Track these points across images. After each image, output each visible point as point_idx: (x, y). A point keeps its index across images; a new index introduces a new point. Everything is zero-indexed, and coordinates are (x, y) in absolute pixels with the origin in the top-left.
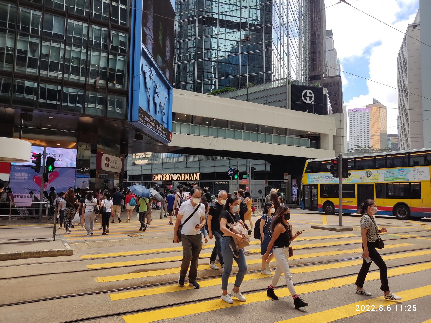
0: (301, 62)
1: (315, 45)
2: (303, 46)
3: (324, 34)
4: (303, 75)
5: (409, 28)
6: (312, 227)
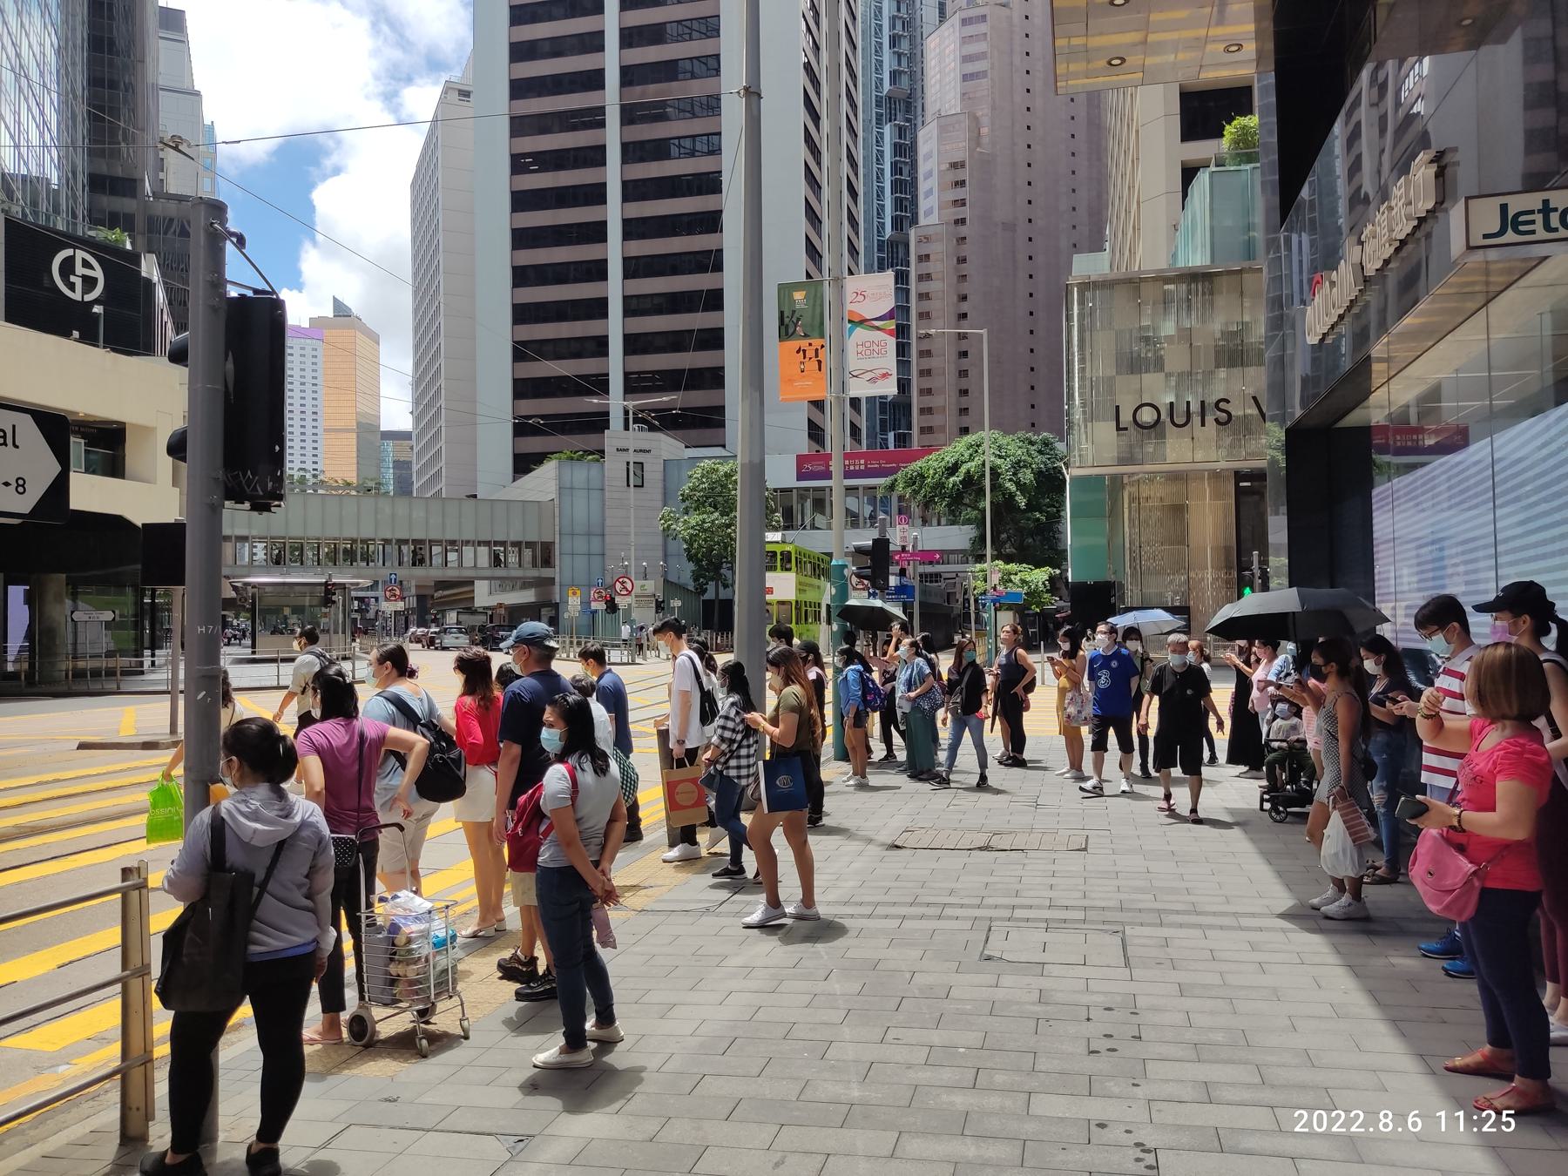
0: (47, 111)
1: (110, 52)
2: (56, 46)
3: (152, 22)
4: (58, 168)
5: (446, 93)
6: (83, 746)
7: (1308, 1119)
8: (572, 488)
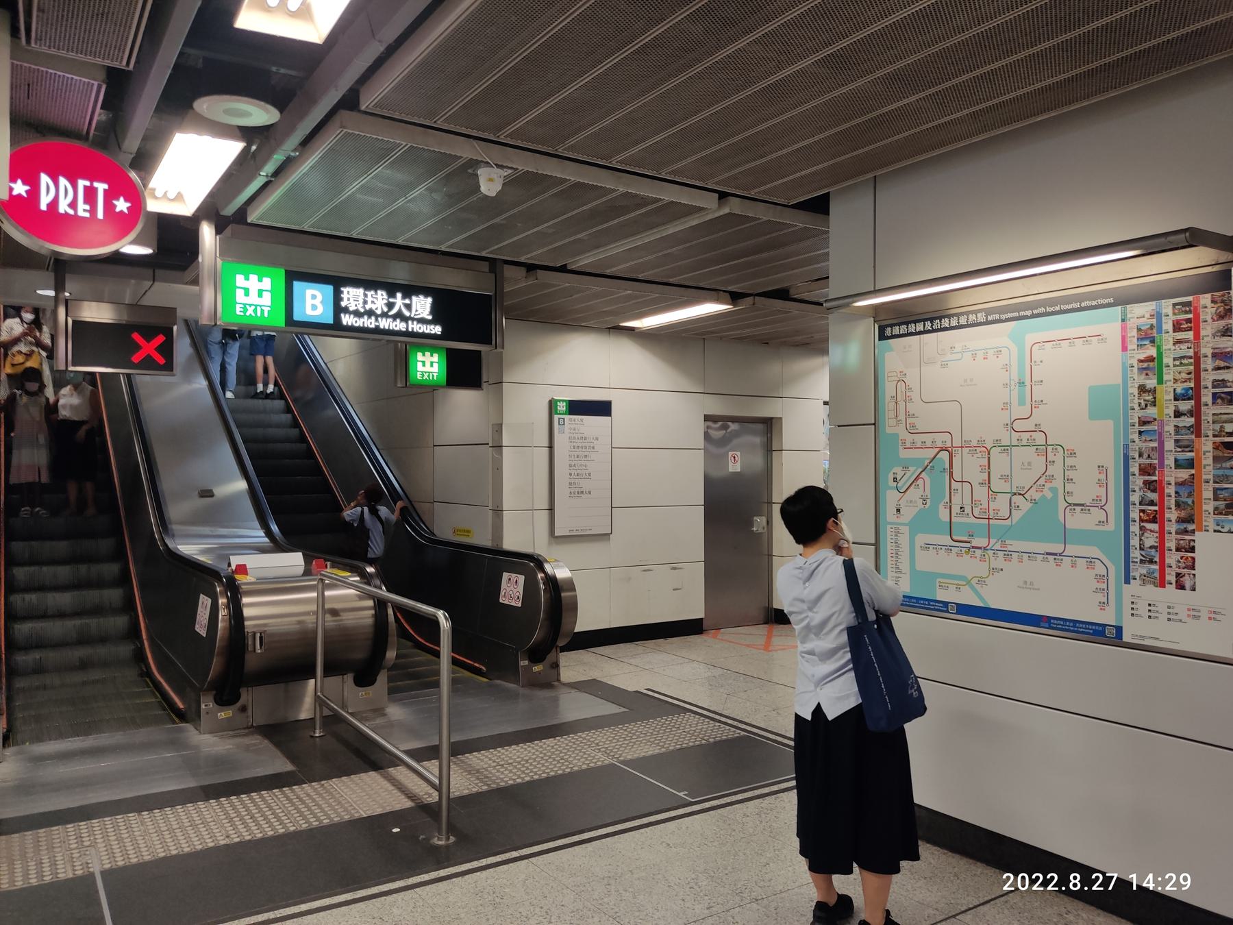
7: (1176, 880)
8: (989, 519)
